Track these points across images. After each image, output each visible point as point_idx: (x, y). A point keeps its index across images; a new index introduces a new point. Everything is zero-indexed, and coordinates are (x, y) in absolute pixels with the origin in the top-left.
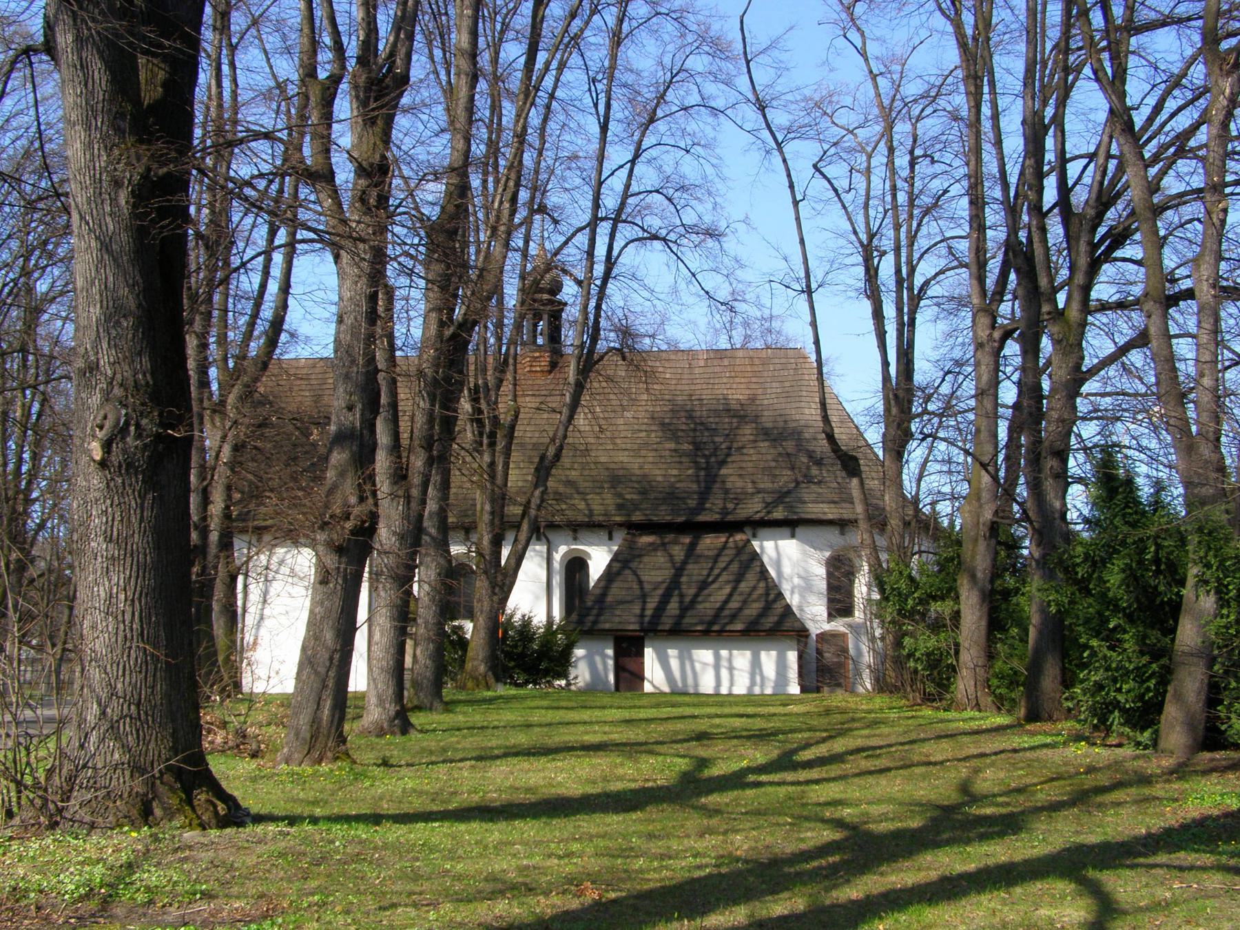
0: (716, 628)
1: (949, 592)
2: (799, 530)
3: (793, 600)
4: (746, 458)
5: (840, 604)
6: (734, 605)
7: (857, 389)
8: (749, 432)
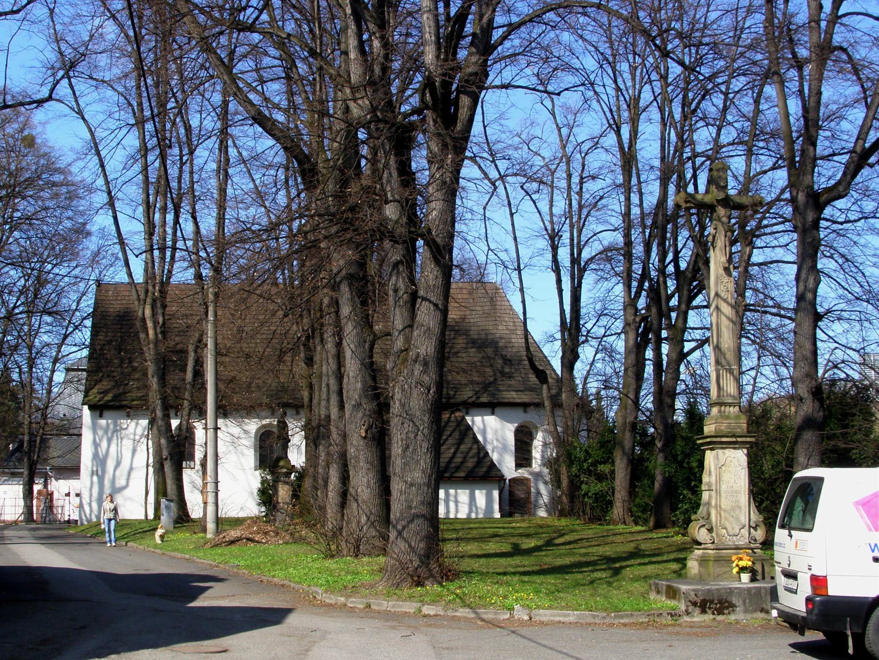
0: (447, 475)
1: (609, 459)
2: (497, 410)
3: (495, 457)
4: (460, 360)
5: (523, 457)
6: (458, 460)
7: (544, 324)
8: (461, 341)
